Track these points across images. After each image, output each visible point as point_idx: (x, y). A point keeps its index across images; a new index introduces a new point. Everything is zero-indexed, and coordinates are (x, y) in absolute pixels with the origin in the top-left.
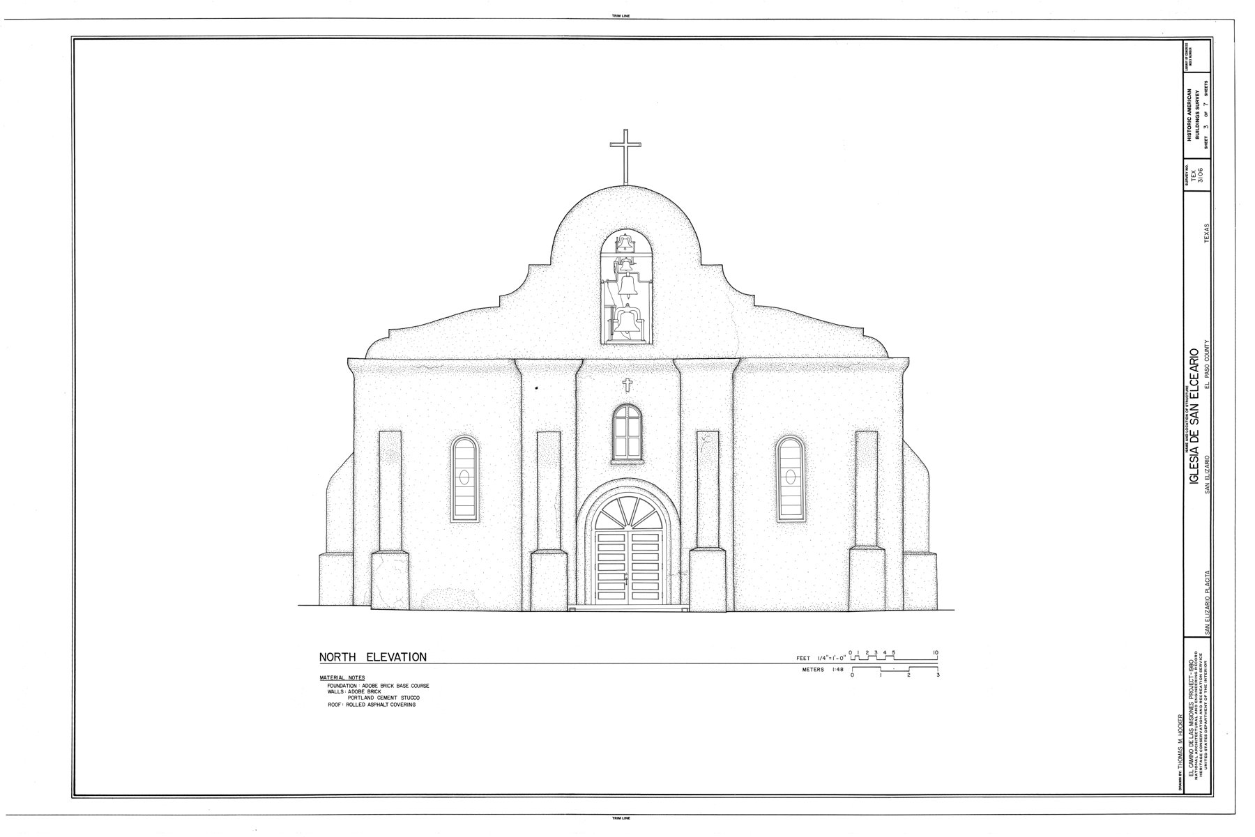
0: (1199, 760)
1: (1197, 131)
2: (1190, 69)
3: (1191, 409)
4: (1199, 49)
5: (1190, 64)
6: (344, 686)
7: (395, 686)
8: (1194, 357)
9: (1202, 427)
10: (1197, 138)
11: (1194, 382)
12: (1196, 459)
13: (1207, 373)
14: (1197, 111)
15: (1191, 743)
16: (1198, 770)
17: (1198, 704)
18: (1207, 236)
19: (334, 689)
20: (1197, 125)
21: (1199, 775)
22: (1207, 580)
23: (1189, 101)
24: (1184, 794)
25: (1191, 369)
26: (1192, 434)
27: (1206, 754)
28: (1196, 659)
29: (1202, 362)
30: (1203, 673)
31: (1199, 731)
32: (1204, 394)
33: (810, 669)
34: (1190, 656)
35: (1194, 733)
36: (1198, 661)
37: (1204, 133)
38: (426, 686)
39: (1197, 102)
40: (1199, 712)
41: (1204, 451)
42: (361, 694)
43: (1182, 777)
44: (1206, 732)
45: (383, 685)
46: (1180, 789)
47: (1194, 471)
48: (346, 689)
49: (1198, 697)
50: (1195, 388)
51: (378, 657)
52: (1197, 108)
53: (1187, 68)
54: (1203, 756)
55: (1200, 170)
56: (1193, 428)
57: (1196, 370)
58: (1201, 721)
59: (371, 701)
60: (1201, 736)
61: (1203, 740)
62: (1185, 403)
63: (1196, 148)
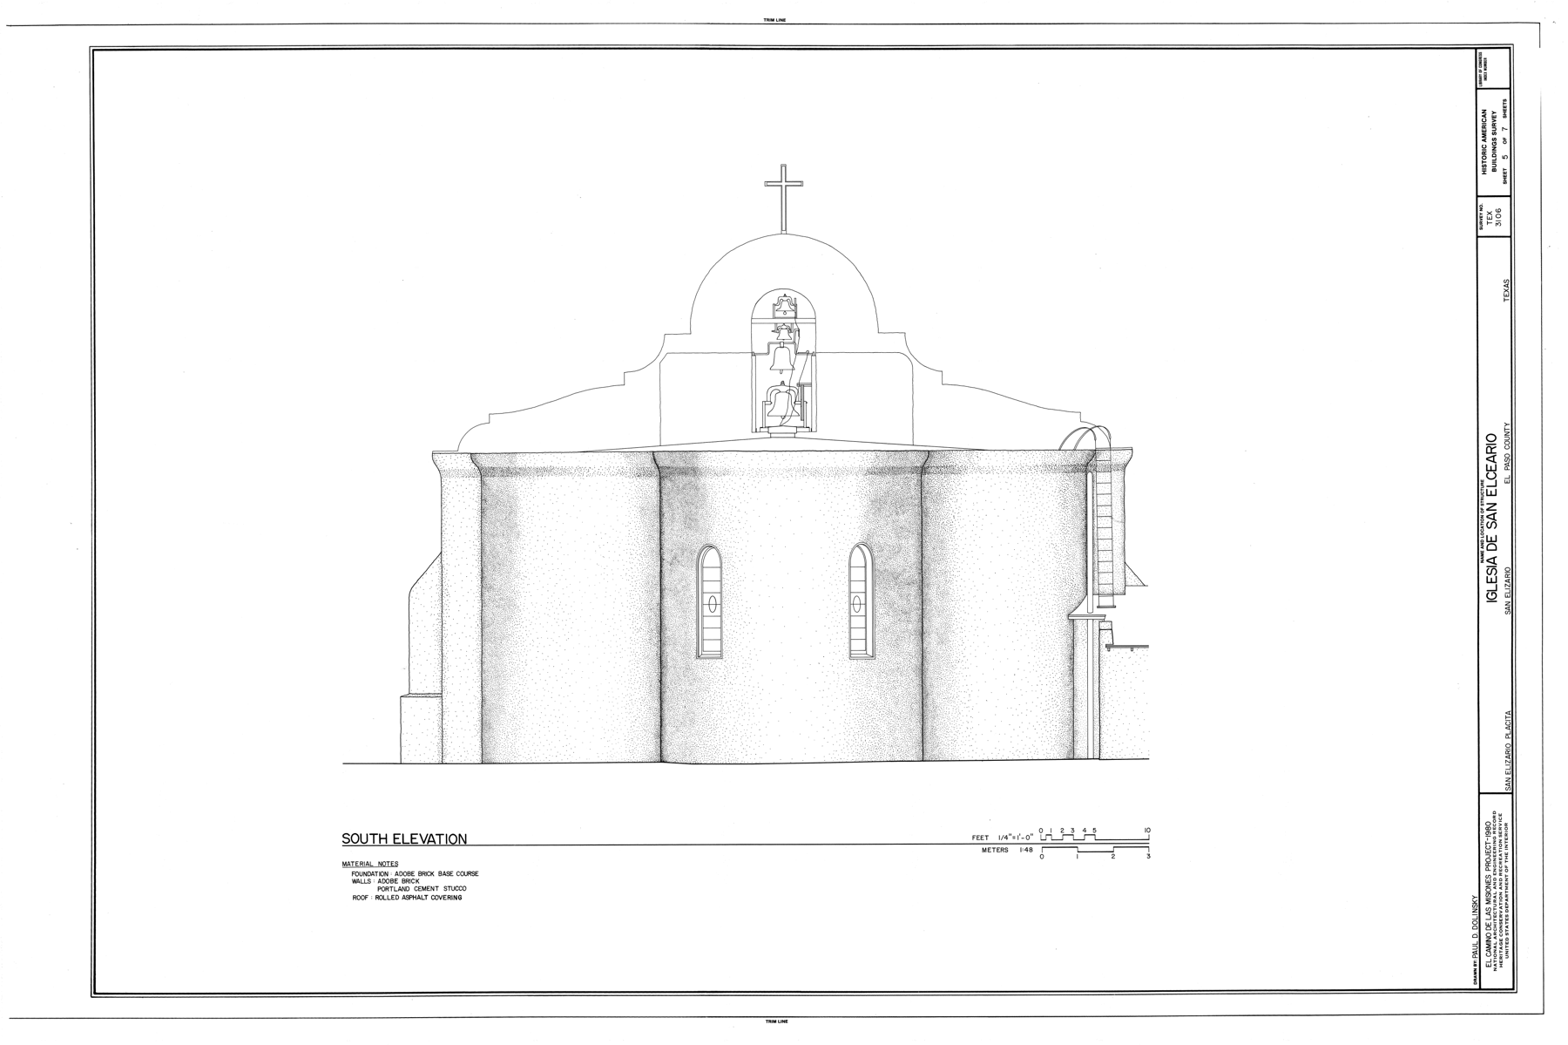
0: (1498, 946)
1: (1494, 162)
2: (1485, 84)
3: (1488, 510)
4: (1496, 60)
5: (1485, 79)
6: (372, 874)
7: (436, 874)
8: (1491, 446)
9: (1502, 532)
10: (1494, 170)
11: (1491, 475)
12: (1494, 571)
13: (1507, 465)
14: (1494, 136)
15: (1488, 926)
16: (1498, 960)
17: (1498, 877)
18: (1506, 293)
19: (359, 877)
20: (1494, 155)
21: (1498, 965)
22: (1508, 723)
23: (1483, 125)
24: (1480, 989)
25: (1487, 459)
26: (1489, 539)
27: (1507, 939)
28: (1494, 821)
29: (1501, 451)
30: (1503, 838)
31: (1498, 910)
32: (1504, 490)
33: (992, 850)
34: (1486, 817)
35: (1492, 914)
36: (1497, 823)
37: (1503, 164)
38: (475, 874)
39: (1494, 125)
40: (1498, 886)
41: (1503, 562)
42: (394, 885)
43: (1477, 967)
44: (1507, 911)
45: (421, 874)
46: (1475, 983)
47: (1492, 587)
48: (375, 879)
49: (1498, 868)
50: (1493, 483)
51: (407, 839)
52: (1494, 133)
53: (1481, 83)
54: (1504, 942)
55: (1498, 211)
56: (1490, 533)
57: (1494, 461)
58: (1501, 899)
59: (406, 893)
60: (1501, 916)
61: (1504, 921)
62: (1479, 501)
63: (1492, 183)
